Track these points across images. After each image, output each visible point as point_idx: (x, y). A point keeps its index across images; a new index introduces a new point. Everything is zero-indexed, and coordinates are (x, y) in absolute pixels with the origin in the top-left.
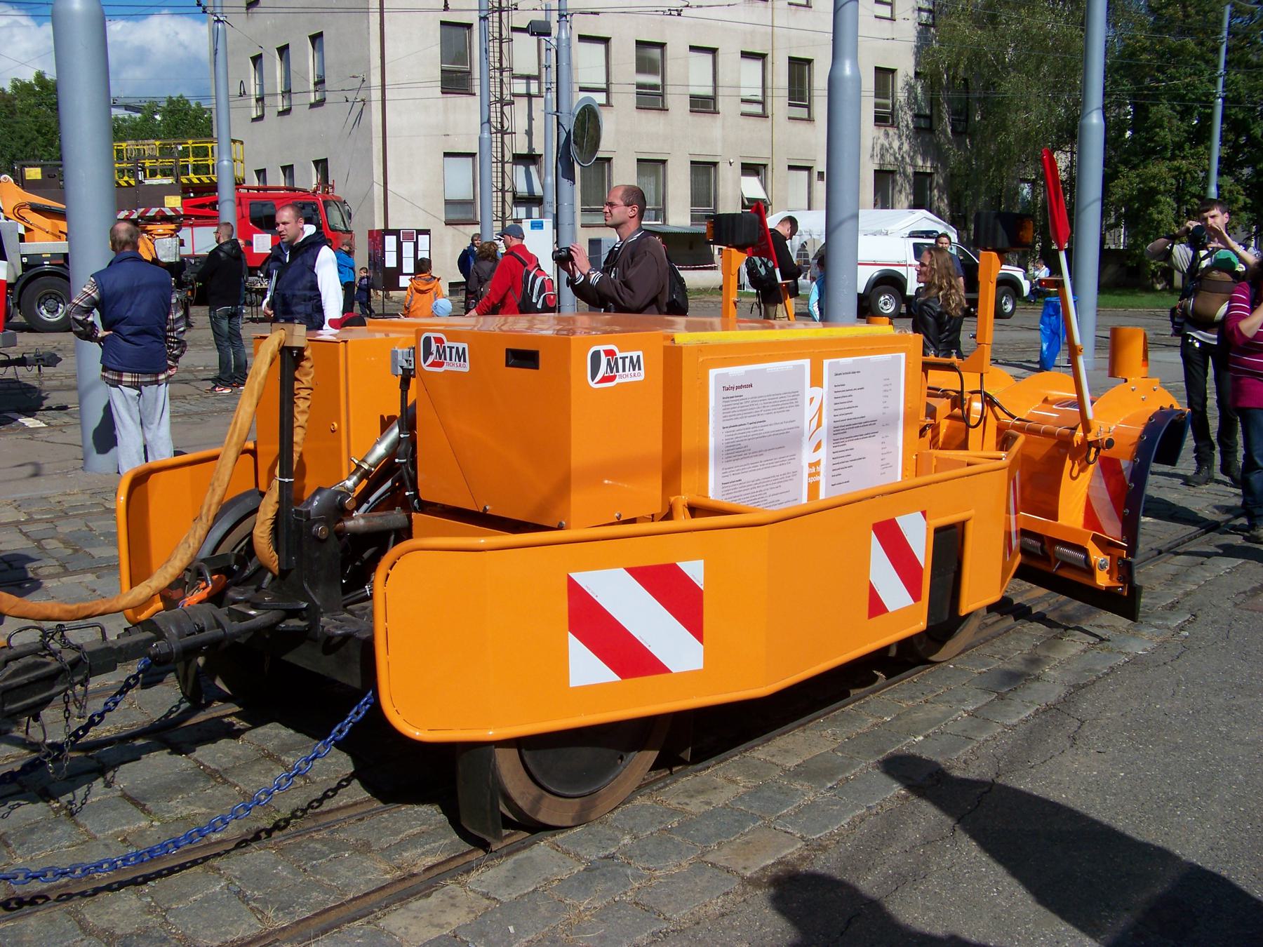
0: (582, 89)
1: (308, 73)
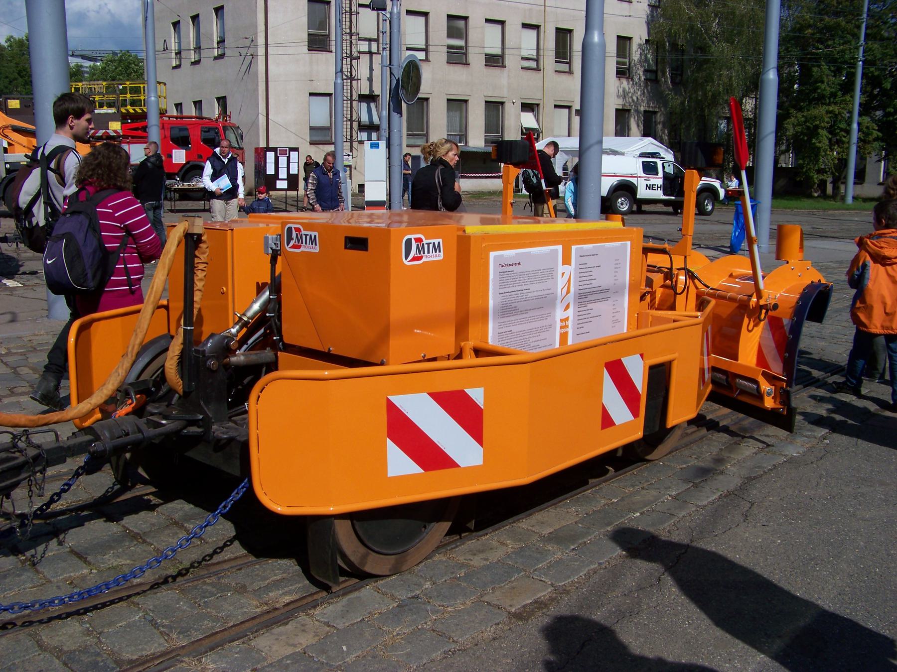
0: (408, 49)
1: (212, 34)
